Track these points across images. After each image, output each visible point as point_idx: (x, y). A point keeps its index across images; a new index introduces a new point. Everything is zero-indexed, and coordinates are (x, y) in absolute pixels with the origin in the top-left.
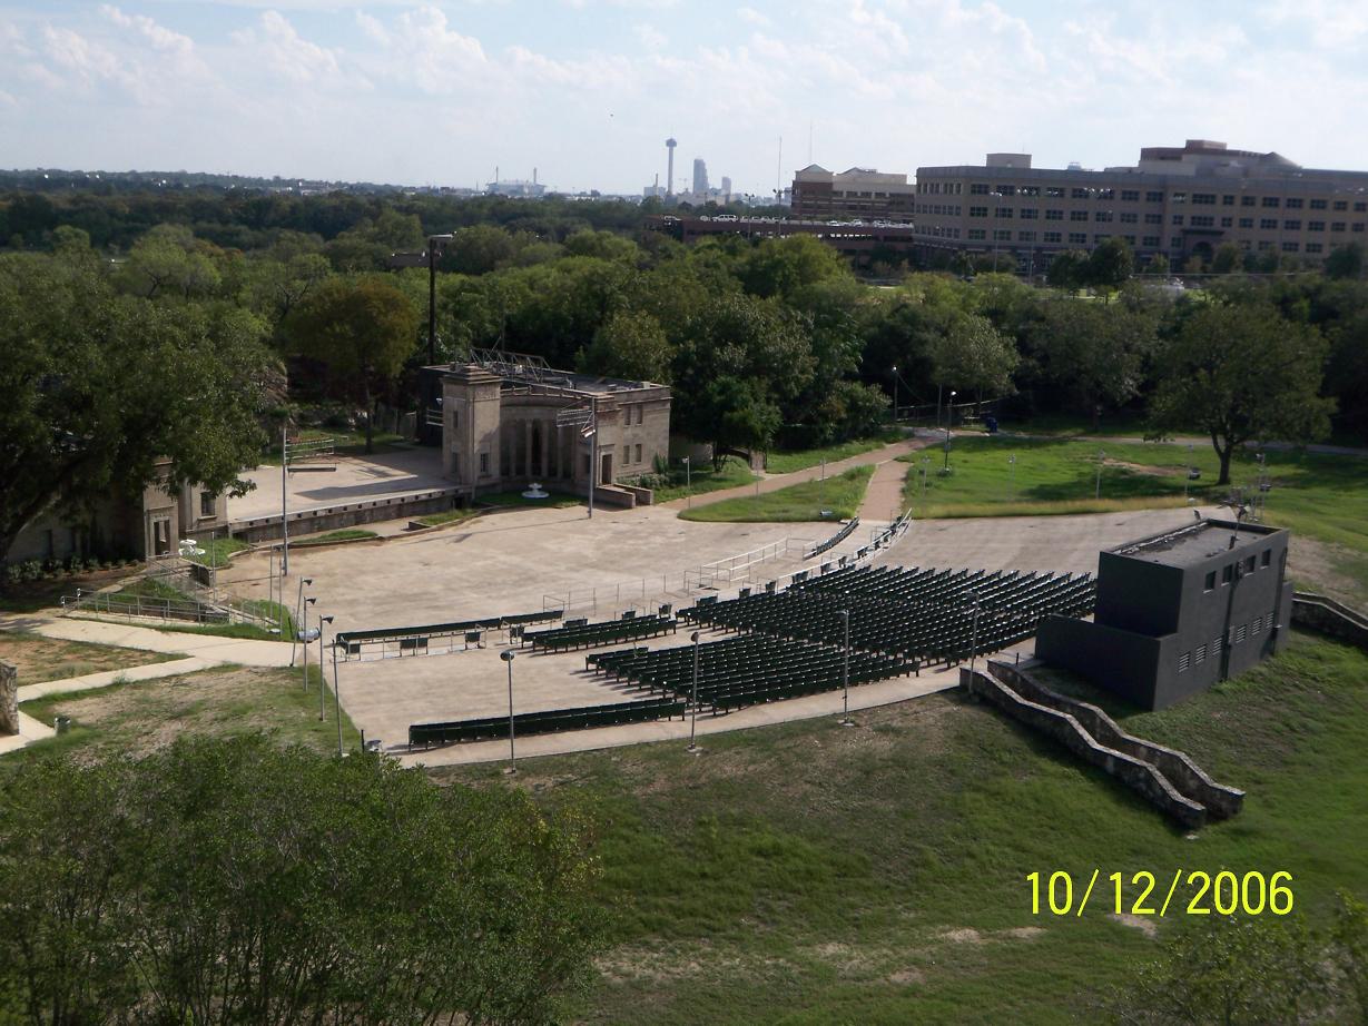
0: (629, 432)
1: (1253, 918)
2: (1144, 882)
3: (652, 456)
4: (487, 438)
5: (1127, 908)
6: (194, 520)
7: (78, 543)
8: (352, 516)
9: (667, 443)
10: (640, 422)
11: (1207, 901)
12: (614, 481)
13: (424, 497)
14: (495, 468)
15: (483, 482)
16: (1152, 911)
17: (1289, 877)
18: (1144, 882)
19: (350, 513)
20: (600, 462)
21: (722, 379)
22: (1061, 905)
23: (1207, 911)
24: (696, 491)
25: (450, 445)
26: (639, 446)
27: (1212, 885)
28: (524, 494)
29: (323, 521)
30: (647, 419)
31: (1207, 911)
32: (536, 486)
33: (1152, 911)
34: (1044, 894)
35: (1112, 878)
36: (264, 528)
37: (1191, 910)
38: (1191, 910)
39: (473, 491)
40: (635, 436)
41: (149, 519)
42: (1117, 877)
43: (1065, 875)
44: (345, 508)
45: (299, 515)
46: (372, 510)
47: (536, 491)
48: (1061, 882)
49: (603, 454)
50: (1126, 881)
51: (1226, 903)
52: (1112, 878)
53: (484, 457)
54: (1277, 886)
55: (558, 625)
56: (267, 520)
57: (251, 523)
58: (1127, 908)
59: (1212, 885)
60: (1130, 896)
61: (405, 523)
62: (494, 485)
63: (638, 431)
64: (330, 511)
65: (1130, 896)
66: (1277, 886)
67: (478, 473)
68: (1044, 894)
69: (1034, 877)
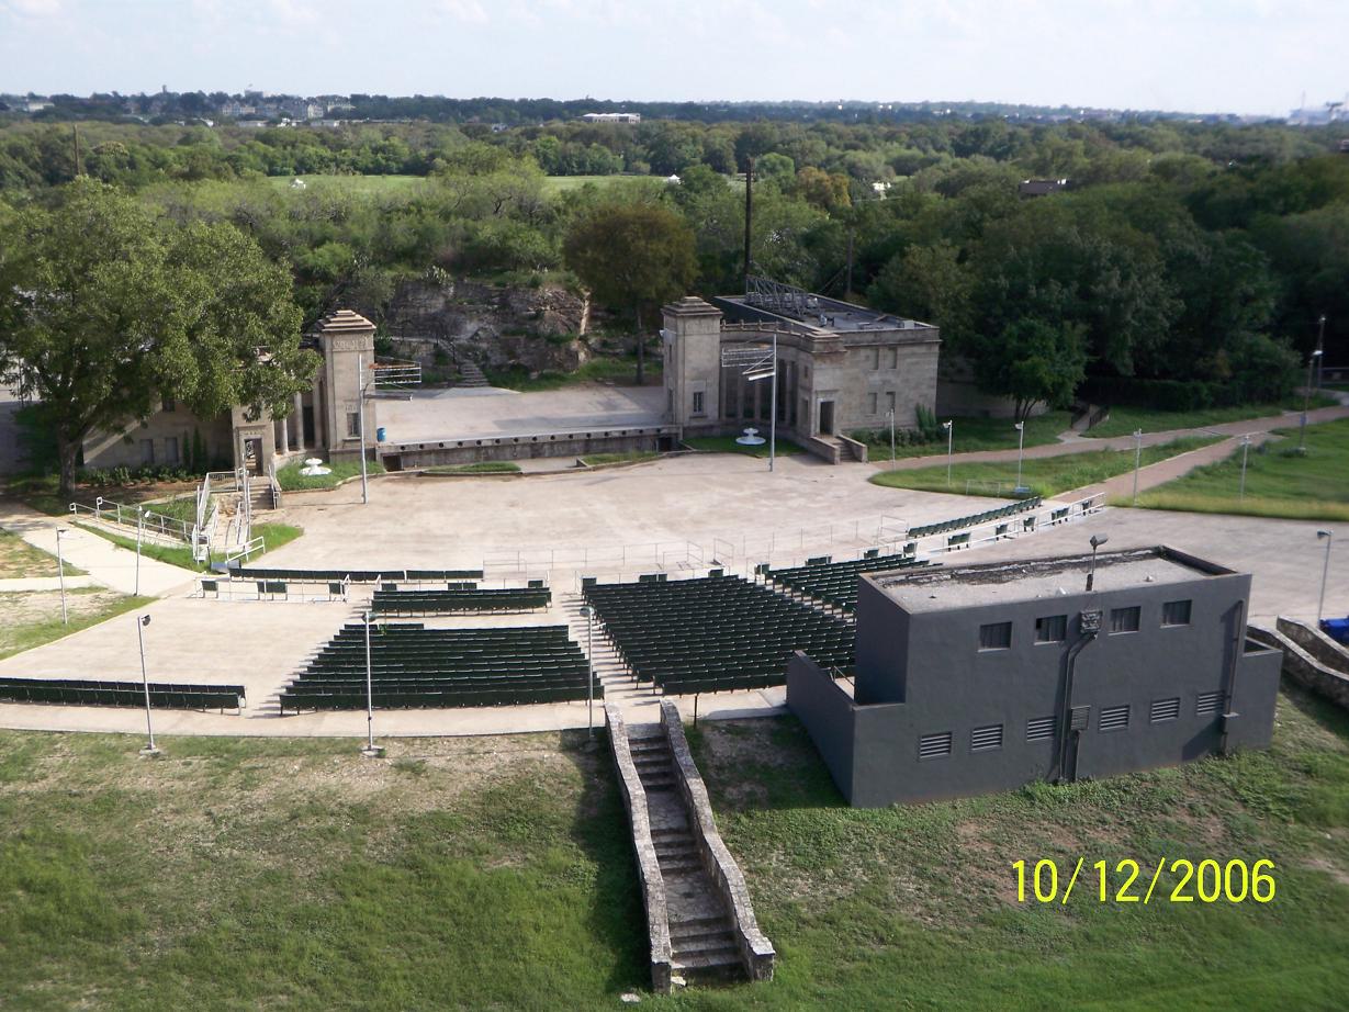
0: (876, 378)
1: (1232, 905)
2: (1128, 870)
3: (912, 405)
4: (702, 375)
5: (1112, 891)
6: (339, 439)
7: (180, 454)
8: (527, 449)
9: (933, 392)
10: (895, 367)
11: (1190, 888)
12: (837, 430)
13: (617, 435)
14: (711, 409)
15: (695, 423)
16: (1136, 899)
17: (1271, 865)
18: (1128, 870)
19: (524, 445)
20: (815, 410)
21: (1026, 321)
22: (1046, 893)
23: (1191, 899)
24: (899, 455)
25: (668, 382)
26: (891, 393)
27: (1196, 873)
28: (739, 440)
29: (491, 452)
30: (903, 365)
31: (1191, 899)
32: (751, 431)
33: (1136, 899)
34: (1029, 877)
35: (1096, 866)
36: (420, 453)
37: (1174, 898)
38: (1119, 898)
39: (681, 431)
40: (885, 382)
41: (238, 436)
42: (1101, 865)
43: (1051, 864)
44: (516, 440)
45: (460, 443)
46: (552, 444)
47: (751, 438)
48: (1045, 871)
49: (821, 400)
50: (1110, 869)
51: (1210, 889)
52: (1096, 866)
53: (699, 398)
54: (1260, 873)
55: (441, 586)
56: (422, 446)
57: (403, 448)
58: (1112, 891)
59: (1196, 873)
60: (1114, 882)
61: (572, 462)
62: (712, 427)
63: (890, 376)
64: (498, 441)
65: (1114, 882)
66: (1260, 873)
67: (690, 413)
68: (1029, 877)
69: (1020, 865)
